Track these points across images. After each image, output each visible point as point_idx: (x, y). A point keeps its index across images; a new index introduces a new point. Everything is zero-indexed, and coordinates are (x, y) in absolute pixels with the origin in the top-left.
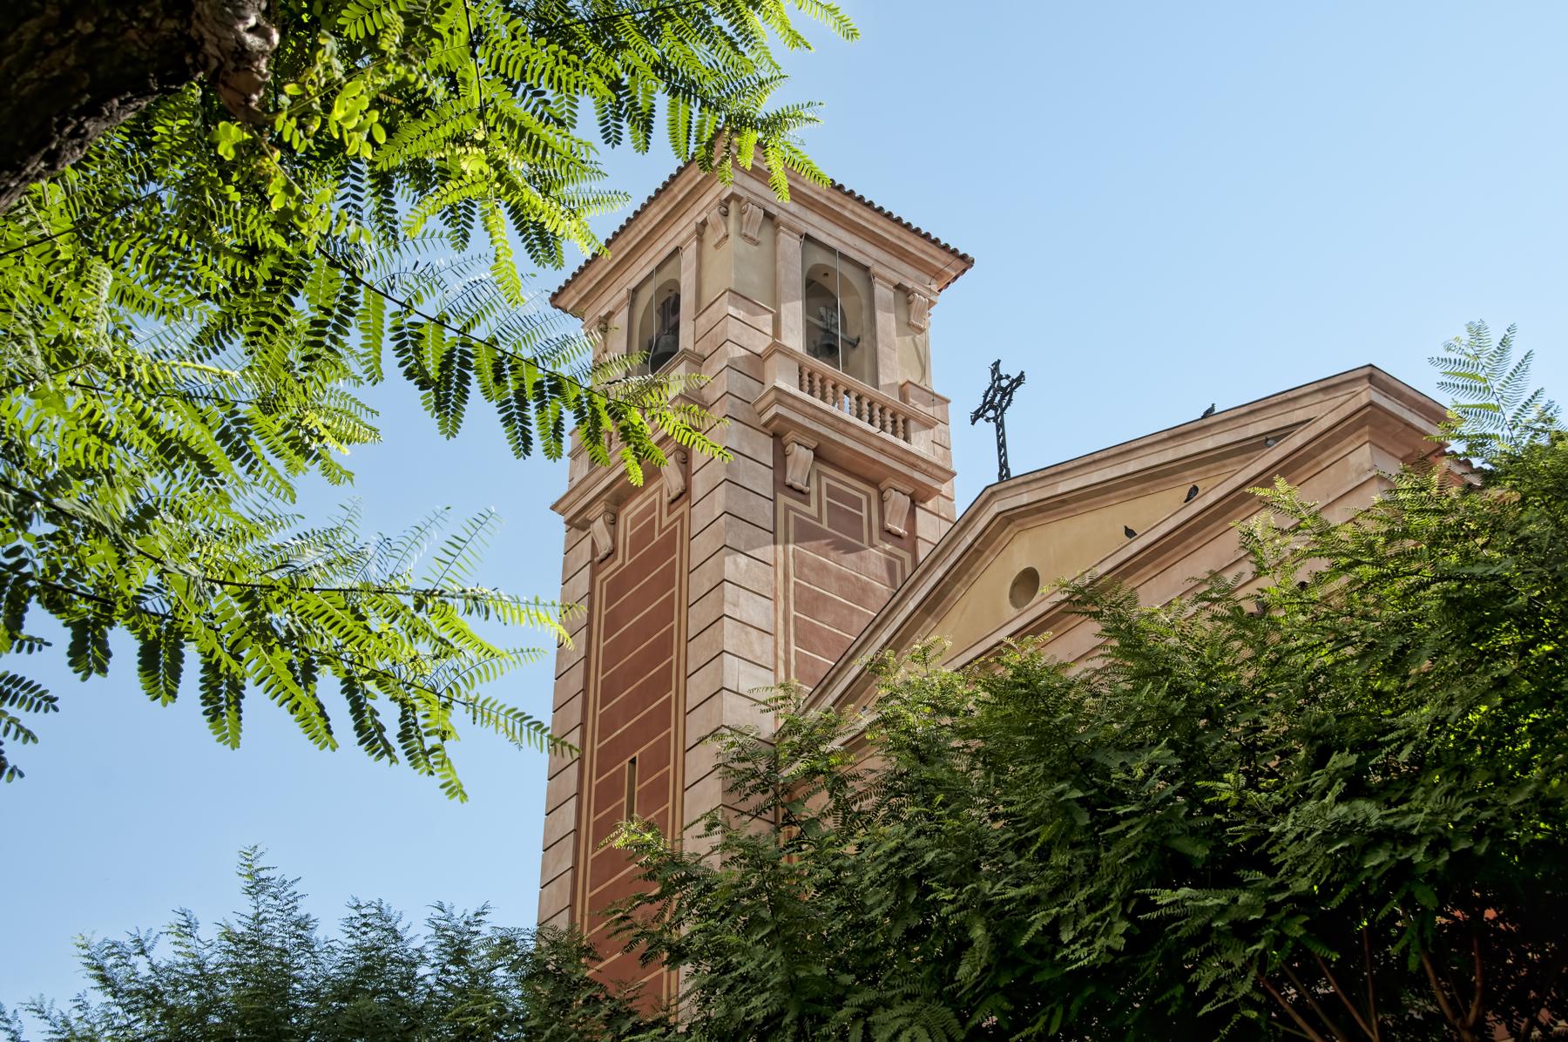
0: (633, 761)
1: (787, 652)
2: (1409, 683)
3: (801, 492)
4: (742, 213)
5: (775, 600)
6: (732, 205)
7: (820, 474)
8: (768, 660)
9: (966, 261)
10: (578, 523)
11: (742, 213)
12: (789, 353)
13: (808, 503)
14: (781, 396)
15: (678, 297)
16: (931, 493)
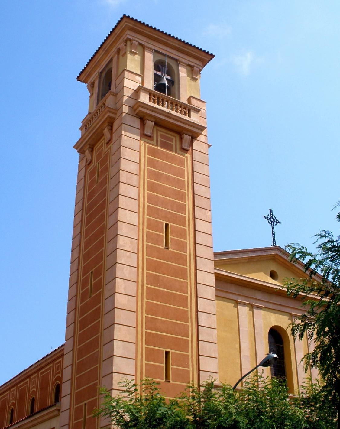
0: (92, 273)
1: (145, 157)
3: (150, 137)
4: (131, 44)
6: (128, 43)
7: (157, 130)
8: (135, 183)
9: (212, 56)
10: (81, 151)
12: (147, 90)
13: (153, 141)
14: (143, 105)
15: (112, 71)
16: (199, 134)
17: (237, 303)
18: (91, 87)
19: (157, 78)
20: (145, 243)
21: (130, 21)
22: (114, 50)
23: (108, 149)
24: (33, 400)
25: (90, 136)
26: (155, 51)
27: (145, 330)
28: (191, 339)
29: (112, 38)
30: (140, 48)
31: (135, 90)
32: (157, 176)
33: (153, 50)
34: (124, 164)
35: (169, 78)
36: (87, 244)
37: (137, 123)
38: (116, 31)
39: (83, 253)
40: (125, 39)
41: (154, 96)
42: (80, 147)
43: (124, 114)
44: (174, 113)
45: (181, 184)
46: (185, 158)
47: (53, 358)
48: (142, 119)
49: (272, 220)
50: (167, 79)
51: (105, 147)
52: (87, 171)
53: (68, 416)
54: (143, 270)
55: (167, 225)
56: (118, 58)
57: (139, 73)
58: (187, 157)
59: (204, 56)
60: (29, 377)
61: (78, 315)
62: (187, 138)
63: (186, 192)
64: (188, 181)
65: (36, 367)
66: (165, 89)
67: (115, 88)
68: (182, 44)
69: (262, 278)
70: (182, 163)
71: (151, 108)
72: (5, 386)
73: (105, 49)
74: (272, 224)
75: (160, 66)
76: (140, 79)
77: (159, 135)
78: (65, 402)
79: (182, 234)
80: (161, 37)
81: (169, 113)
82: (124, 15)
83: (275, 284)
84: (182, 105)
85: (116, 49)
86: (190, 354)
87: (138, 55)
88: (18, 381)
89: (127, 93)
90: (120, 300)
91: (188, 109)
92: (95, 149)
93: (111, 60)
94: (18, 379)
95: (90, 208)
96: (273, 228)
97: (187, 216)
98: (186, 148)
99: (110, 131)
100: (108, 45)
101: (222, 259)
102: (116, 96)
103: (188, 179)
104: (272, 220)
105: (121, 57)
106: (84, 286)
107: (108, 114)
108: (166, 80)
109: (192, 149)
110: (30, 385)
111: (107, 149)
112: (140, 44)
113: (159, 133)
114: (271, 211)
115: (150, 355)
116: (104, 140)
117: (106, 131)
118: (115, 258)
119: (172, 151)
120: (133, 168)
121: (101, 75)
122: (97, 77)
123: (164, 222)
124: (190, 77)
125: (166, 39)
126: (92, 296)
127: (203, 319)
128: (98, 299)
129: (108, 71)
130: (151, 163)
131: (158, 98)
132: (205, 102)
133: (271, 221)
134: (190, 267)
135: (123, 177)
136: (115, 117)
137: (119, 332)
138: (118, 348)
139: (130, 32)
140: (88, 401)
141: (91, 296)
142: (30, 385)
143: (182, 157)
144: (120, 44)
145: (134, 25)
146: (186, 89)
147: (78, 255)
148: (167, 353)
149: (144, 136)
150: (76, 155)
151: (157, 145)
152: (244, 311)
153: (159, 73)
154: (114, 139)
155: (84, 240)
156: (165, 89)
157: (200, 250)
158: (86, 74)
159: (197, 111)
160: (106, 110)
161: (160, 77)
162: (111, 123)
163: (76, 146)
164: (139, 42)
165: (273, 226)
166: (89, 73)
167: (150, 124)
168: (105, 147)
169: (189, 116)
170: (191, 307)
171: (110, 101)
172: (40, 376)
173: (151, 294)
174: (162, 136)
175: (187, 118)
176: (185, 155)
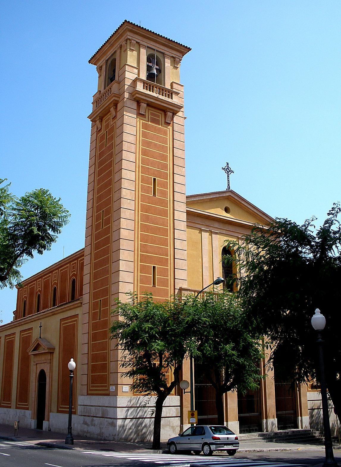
0: (103, 211)
1: (140, 130)
2: (165, 308)
3: (143, 115)
4: (130, 43)
5: (134, 262)
6: (128, 41)
8: (133, 151)
9: (189, 49)
11: (130, 43)
12: (141, 80)
15: (116, 60)
17: (201, 231)
18: (100, 69)
19: (149, 68)
20: (140, 193)
21: (130, 25)
22: (117, 45)
23: (114, 123)
24: (55, 289)
25: (100, 111)
26: (148, 47)
27: (139, 253)
28: (170, 258)
29: (116, 36)
30: (137, 45)
31: (133, 79)
32: (148, 144)
33: (146, 47)
34: (125, 137)
35: (158, 67)
36: (99, 191)
37: (135, 105)
38: (119, 31)
39: (96, 196)
40: (126, 38)
41: (147, 84)
42: (93, 118)
43: (125, 99)
44: (160, 97)
45: (165, 149)
46: (168, 129)
47: (70, 260)
48: (138, 102)
49: (228, 170)
50: (156, 69)
51: (111, 121)
52: (98, 135)
53: (88, 307)
54: (138, 211)
55: (155, 179)
56: (120, 52)
57: (136, 66)
58: (169, 129)
59: (184, 50)
60: (51, 272)
61: (94, 240)
62: (170, 114)
63: (168, 155)
64: (169, 146)
65: (57, 265)
66: (154, 77)
67: (119, 77)
68: (168, 41)
69: (219, 212)
70: (165, 133)
71: (145, 95)
72: (34, 277)
73: (110, 43)
74: (228, 173)
75: (151, 59)
76: (136, 71)
77: (150, 113)
78: (86, 298)
79: (165, 185)
80: (153, 36)
81: (157, 98)
82: (126, 21)
83: (228, 216)
84: (166, 90)
85: (119, 45)
86: (169, 268)
87: (135, 51)
88: (43, 275)
89: (128, 83)
90: (124, 233)
91: (171, 93)
92: (104, 120)
93: (115, 52)
94: (43, 273)
95: (100, 164)
96: (228, 176)
97: (168, 172)
98: (169, 122)
99: (115, 109)
100: (113, 40)
101: (191, 200)
102: (119, 84)
103: (169, 145)
104: (228, 170)
105: (122, 52)
106: (97, 220)
107: (114, 98)
108: (155, 70)
109: (173, 122)
110: (52, 278)
111: (113, 122)
112: (137, 42)
113: (150, 111)
114: (228, 164)
115: (143, 269)
116: (110, 115)
117: (112, 109)
118: (120, 204)
119: (159, 125)
120: (131, 139)
121: (108, 62)
122: (104, 63)
123: (153, 177)
124: (173, 66)
125: (156, 38)
126: (104, 228)
127: (178, 244)
128: (108, 231)
129: (113, 60)
130: (144, 135)
131: (150, 86)
132: (183, 86)
133: (227, 171)
134: (170, 209)
135: (125, 146)
136: (119, 100)
137: (123, 255)
138: (123, 266)
139: (130, 33)
140: (102, 298)
141: (102, 228)
142: (52, 278)
143: (165, 128)
144: (122, 41)
145: (133, 28)
146: (170, 74)
147: (92, 197)
148: (154, 267)
149: (139, 114)
150: (89, 123)
151: (148, 121)
152: (206, 235)
153: (150, 64)
154: (118, 117)
155: (96, 188)
156: (154, 77)
157: (177, 197)
158: (96, 59)
159: (177, 94)
160: (113, 95)
161: (151, 67)
162: (116, 104)
163: (90, 117)
164: (136, 41)
165: (228, 175)
166: (98, 59)
167: (144, 105)
168: (111, 121)
169: (172, 98)
170: (170, 236)
171: (114, 86)
172: (60, 273)
173: (144, 228)
174: (152, 114)
175: (170, 100)
176: (168, 127)
